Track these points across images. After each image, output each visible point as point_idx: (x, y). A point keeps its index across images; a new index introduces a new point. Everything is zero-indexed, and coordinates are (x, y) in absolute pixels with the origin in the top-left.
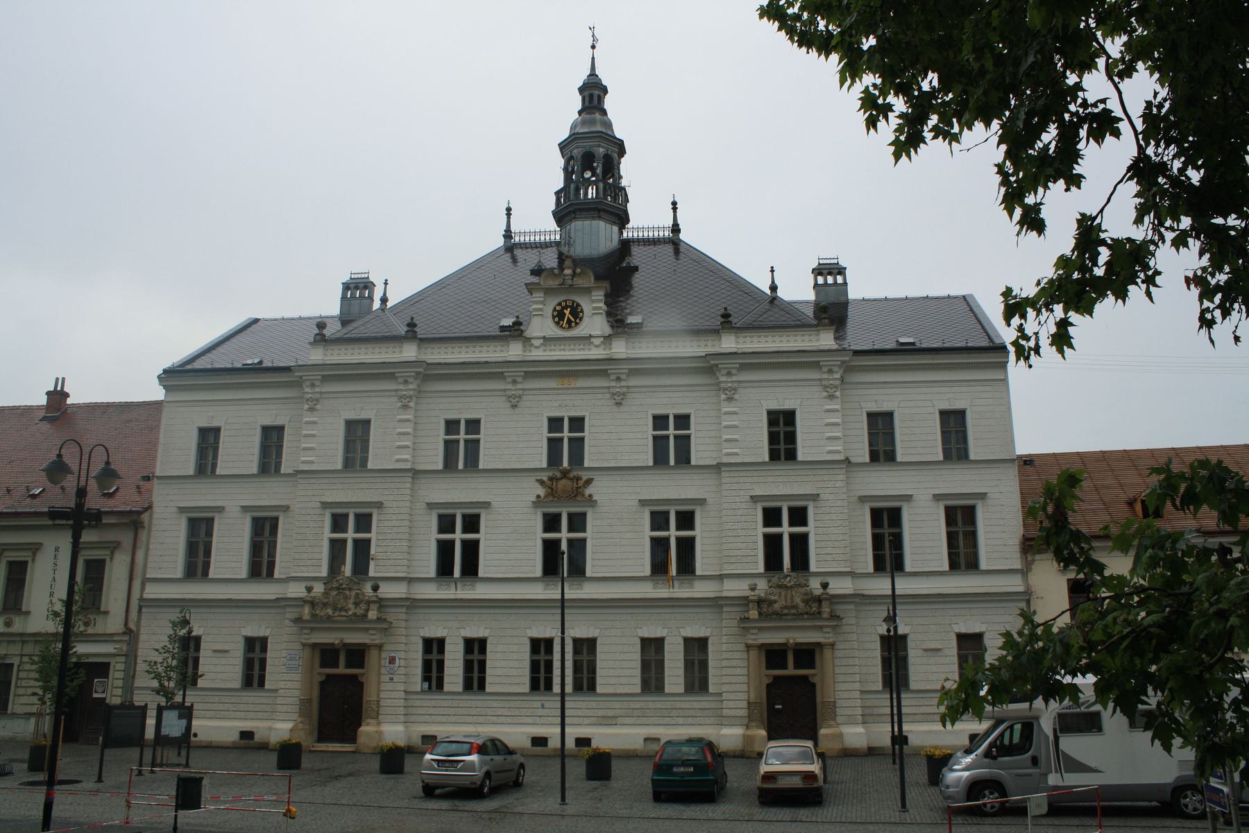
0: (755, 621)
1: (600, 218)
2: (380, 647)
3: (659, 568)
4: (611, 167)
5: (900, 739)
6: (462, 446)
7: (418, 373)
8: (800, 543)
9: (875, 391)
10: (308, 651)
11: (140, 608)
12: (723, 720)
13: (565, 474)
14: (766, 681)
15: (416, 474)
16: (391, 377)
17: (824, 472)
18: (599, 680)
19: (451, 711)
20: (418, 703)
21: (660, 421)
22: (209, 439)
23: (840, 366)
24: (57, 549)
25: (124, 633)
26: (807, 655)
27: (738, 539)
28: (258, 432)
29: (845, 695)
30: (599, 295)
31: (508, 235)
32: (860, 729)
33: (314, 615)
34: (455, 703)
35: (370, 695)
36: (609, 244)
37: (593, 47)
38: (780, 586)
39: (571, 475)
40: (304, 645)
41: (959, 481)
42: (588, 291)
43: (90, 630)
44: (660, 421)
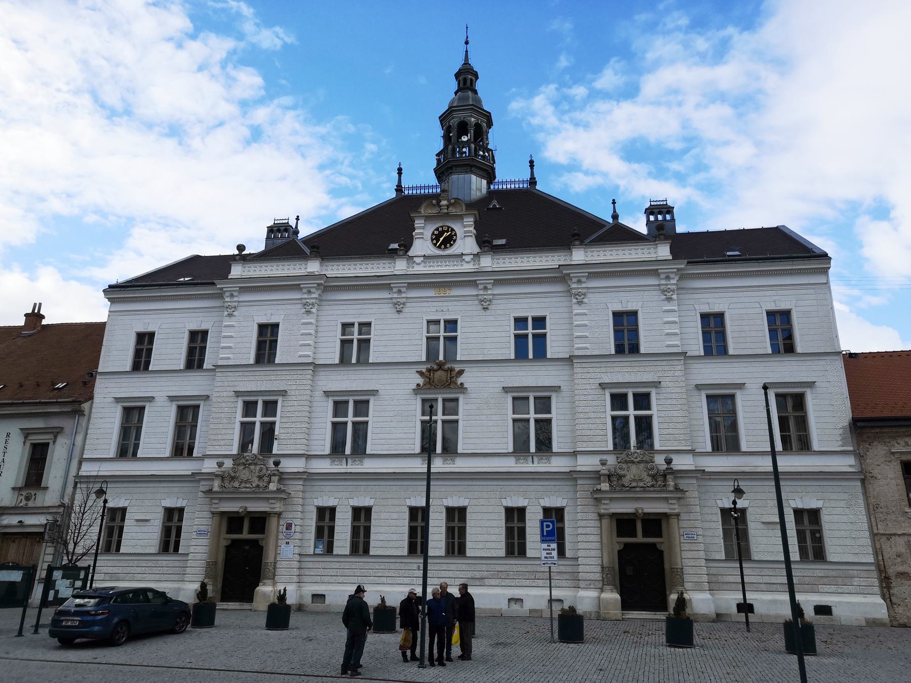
0: (605, 492)
1: (472, 172)
2: (279, 515)
3: (520, 448)
4: (480, 134)
5: (745, 608)
6: (355, 347)
7: (319, 285)
8: (645, 425)
9: (708, 295)
10: (217, 518)
11: (76, 483)
12: (576, 582)
13: (441, 366)
14: (618, 547)
15: (316, 367)
16: (297, 288)
17: (665, 363)
18: (469, 545)
19: (339, 572)
20: (310, 565)
21: (520, 322)
22: (145, 341)
23: (676, 274)
24: (8, 435)
25: (59, 506)
26: (655, 524)
27: (589, 421)
28: (186, 336)
29: (692, 563)
30: (470, 221)
31: (399, 189)
32: (707, 596)
33: (222, 487)
34: (342, 565)
35: (269, 557)
36: (479, 194)
37: (467, 43)
38: (626, 462)
39: (446, 367)
40: (213, 513)
41: (786, 371)
42: (460, 217)
43: (30, 504)
44: (520, 322)
